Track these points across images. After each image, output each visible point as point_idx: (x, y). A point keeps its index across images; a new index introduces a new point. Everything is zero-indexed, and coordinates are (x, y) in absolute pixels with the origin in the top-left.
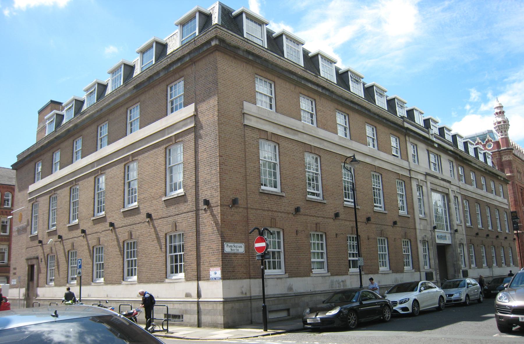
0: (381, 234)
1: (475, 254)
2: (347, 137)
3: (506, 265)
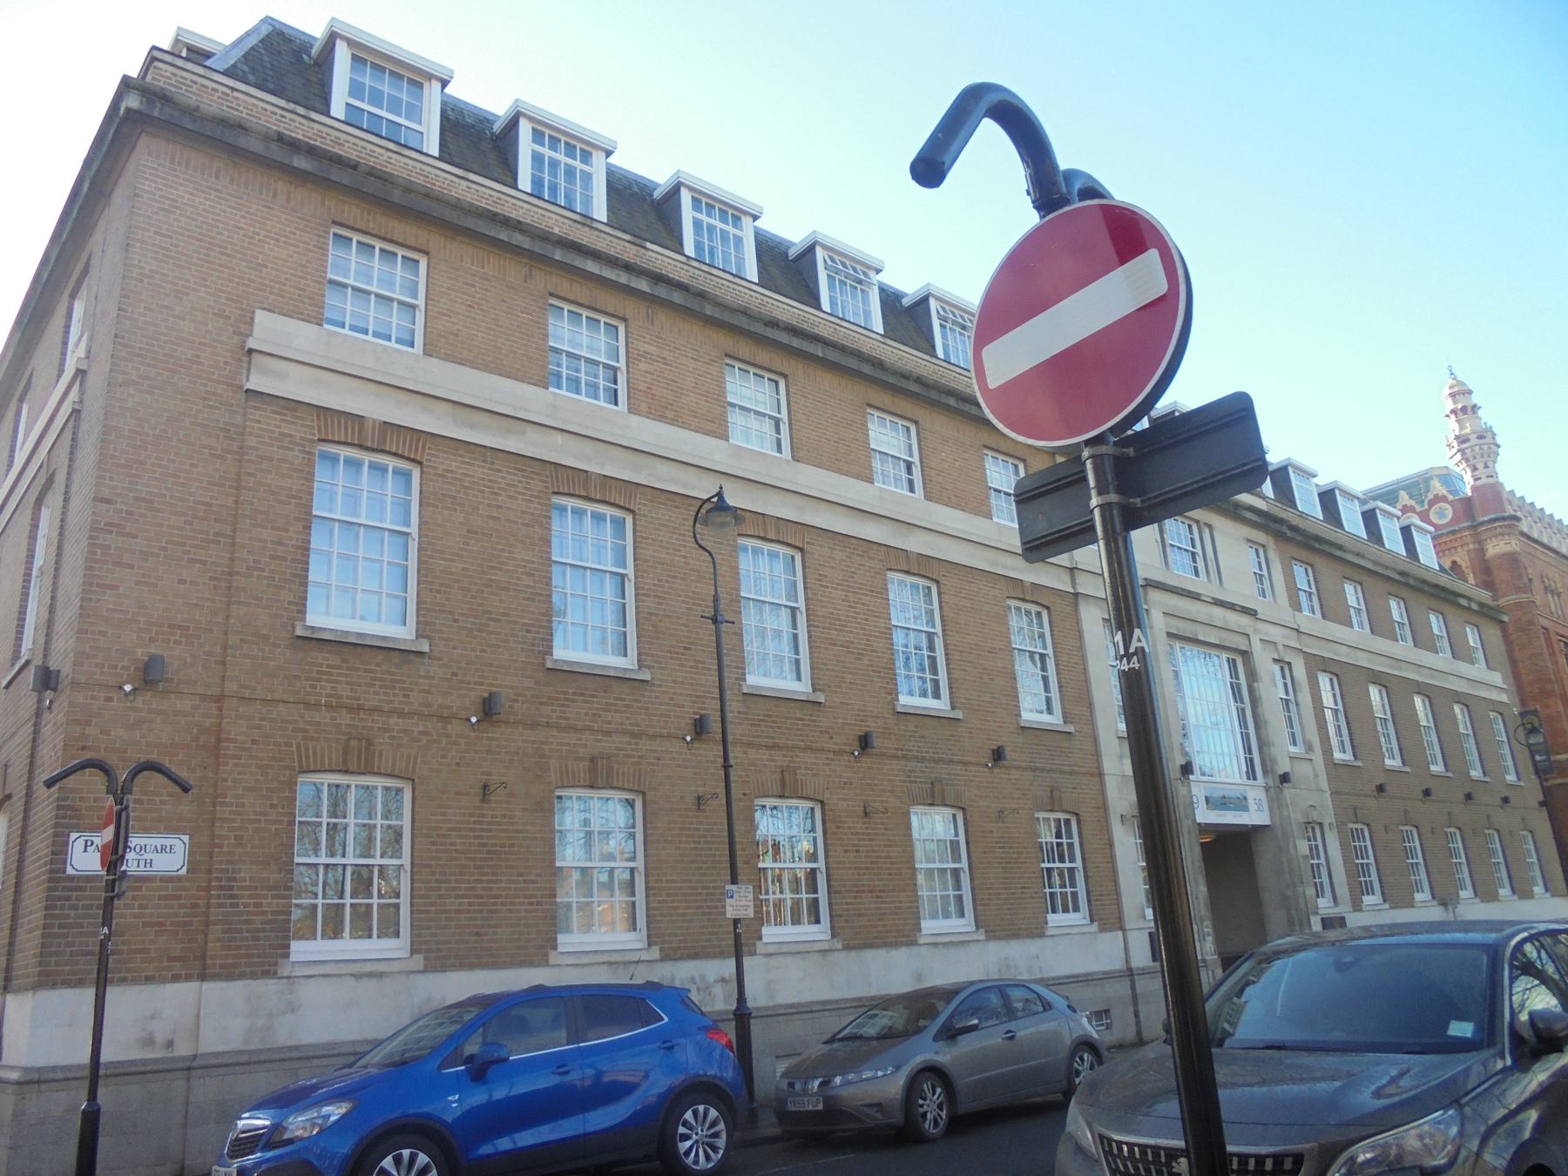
0: (933, 797)
1: (1376, 860)
3: (1547, 890)
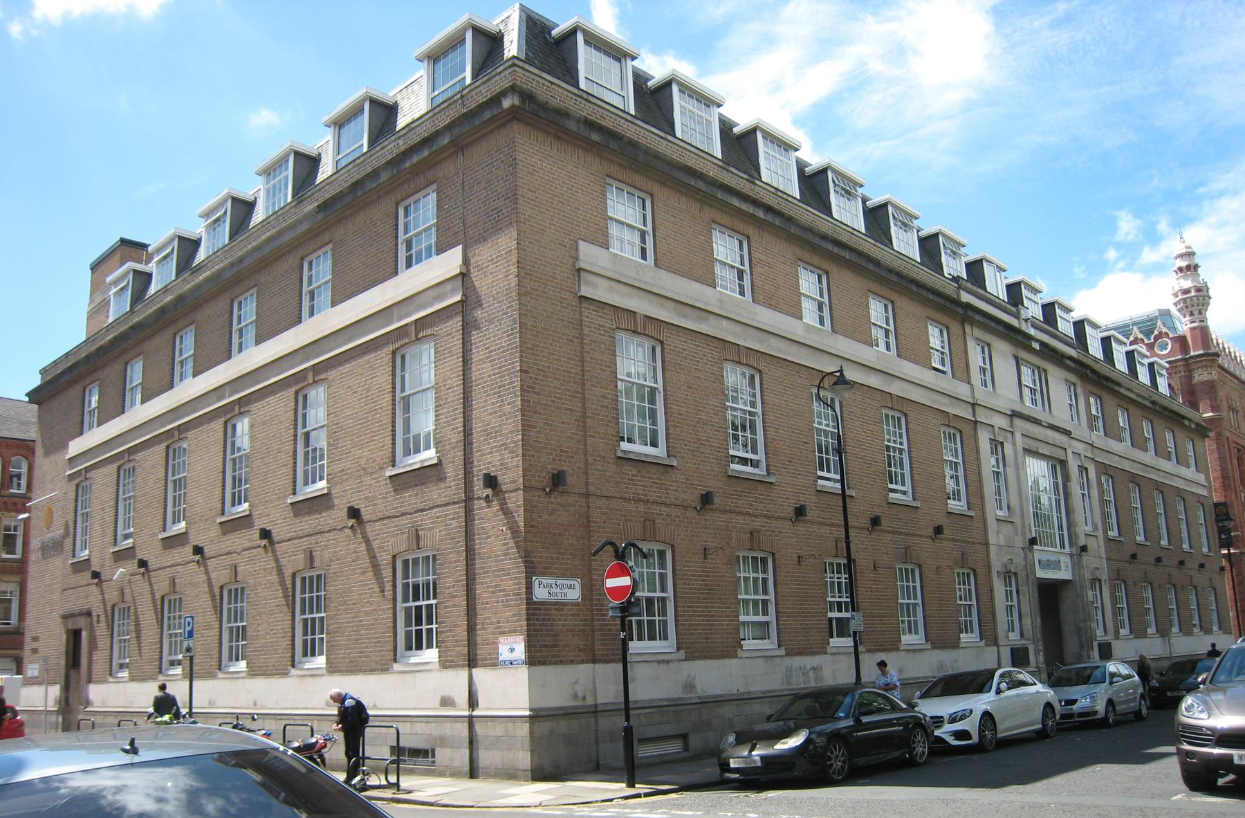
0: (906, 557)
1: (1127, 605)
2: (824, 326)
3: (1201, 630)
